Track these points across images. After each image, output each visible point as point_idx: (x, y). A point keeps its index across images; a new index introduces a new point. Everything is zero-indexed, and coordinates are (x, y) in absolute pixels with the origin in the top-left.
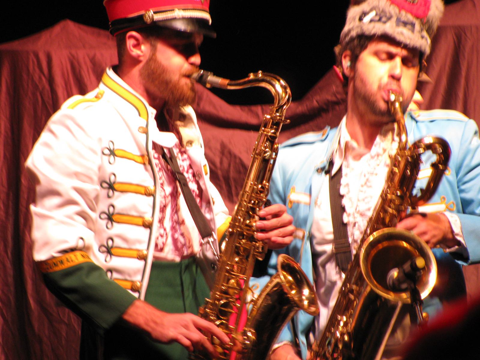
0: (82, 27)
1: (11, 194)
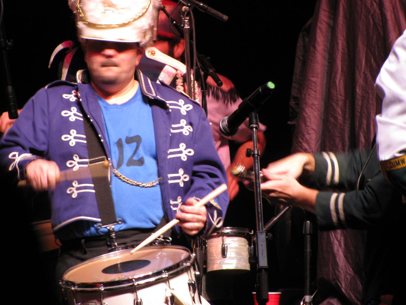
1: (348, 101)
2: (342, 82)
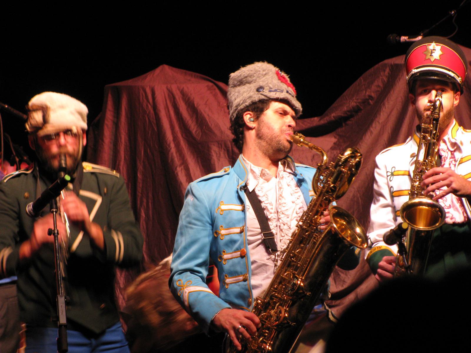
0: (174, 69)
1: (130, 184)
2: (125, 168)
